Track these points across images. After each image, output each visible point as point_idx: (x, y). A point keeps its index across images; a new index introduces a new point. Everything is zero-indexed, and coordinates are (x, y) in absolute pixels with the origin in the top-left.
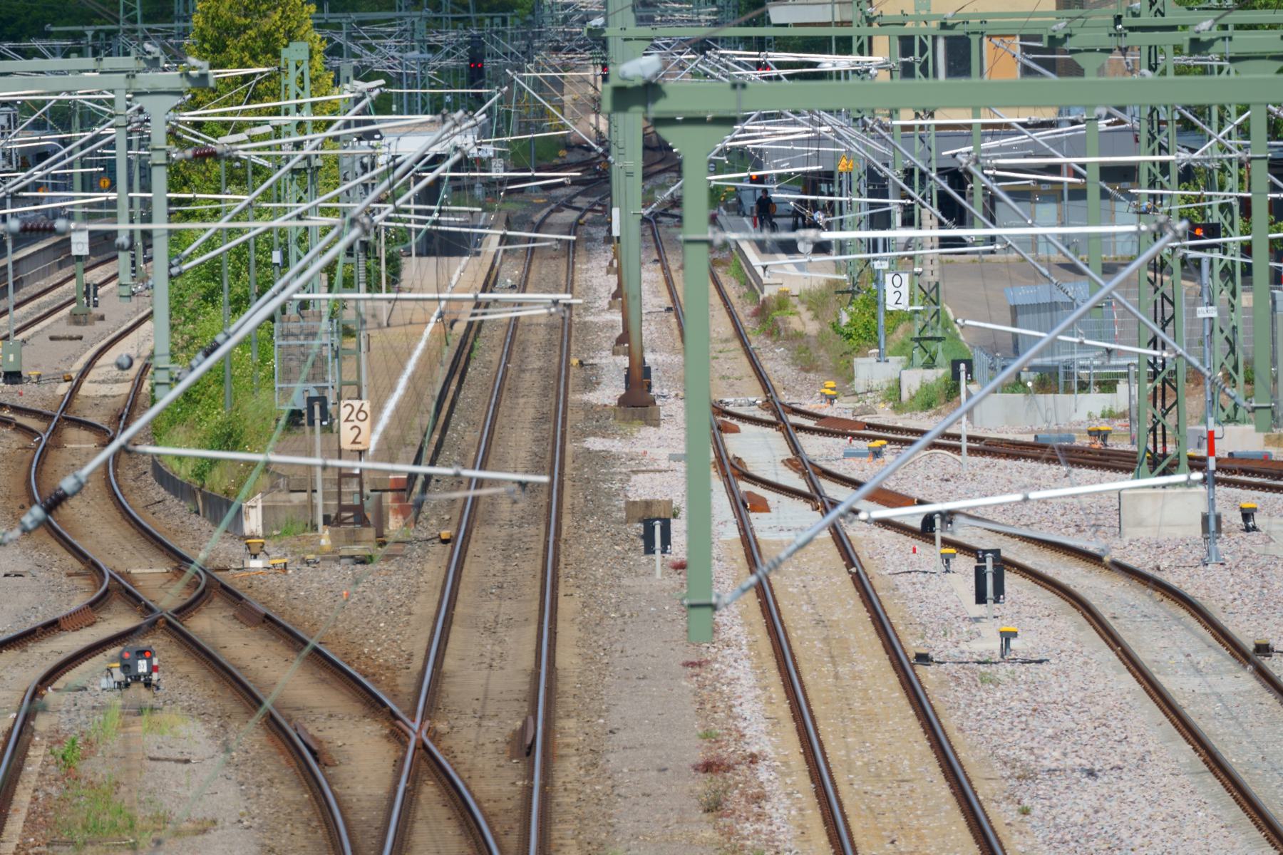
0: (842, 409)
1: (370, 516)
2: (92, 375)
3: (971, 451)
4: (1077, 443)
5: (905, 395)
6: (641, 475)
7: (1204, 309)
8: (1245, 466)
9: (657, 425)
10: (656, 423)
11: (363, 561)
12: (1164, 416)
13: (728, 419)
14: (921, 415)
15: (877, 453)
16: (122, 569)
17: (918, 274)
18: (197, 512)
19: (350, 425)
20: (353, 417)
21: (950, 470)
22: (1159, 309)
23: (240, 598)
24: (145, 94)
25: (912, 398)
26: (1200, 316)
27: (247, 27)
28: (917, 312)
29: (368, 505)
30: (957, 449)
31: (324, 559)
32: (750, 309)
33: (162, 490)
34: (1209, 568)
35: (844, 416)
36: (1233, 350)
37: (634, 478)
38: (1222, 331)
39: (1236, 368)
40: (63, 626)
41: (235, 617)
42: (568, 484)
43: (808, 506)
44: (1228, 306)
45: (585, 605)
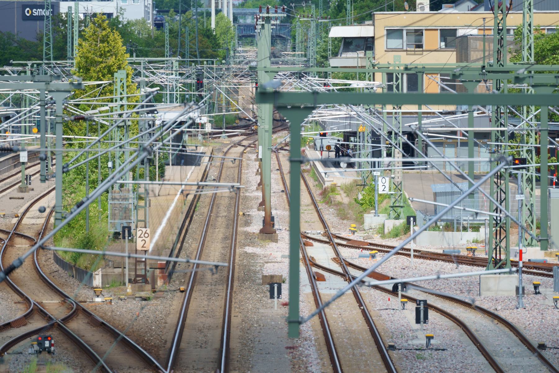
0: (358, 237)
2: (28, 215)
3: (415, 256)
4: (462, 254)
5: (386, 231)
6: (269, 264)
7: (519, 196)
8: (535, 265)
9: (277, 242)
10: (276, 241)
11: (145, 299)
12: (500, 242)
13: (308, 240)
15: (373, 256)
16: (39, 301)
17: (393, 178)
18: (73, 276)
19: (141, 239)
20: (142, 236)
21: (405, 264)
22: (499, 195)
25: (390, 233)
27: (102, 62)
28: (392, 194)
29: (148, 274)
30: (409, 255)
31: (128, 298)
33: (57, 266)
34: (519, 310)
36: (531, 214)
38: (526, 206)
39: (532, 222)
40: (12, 325)
41: (88, 323)
44: (529, 195)
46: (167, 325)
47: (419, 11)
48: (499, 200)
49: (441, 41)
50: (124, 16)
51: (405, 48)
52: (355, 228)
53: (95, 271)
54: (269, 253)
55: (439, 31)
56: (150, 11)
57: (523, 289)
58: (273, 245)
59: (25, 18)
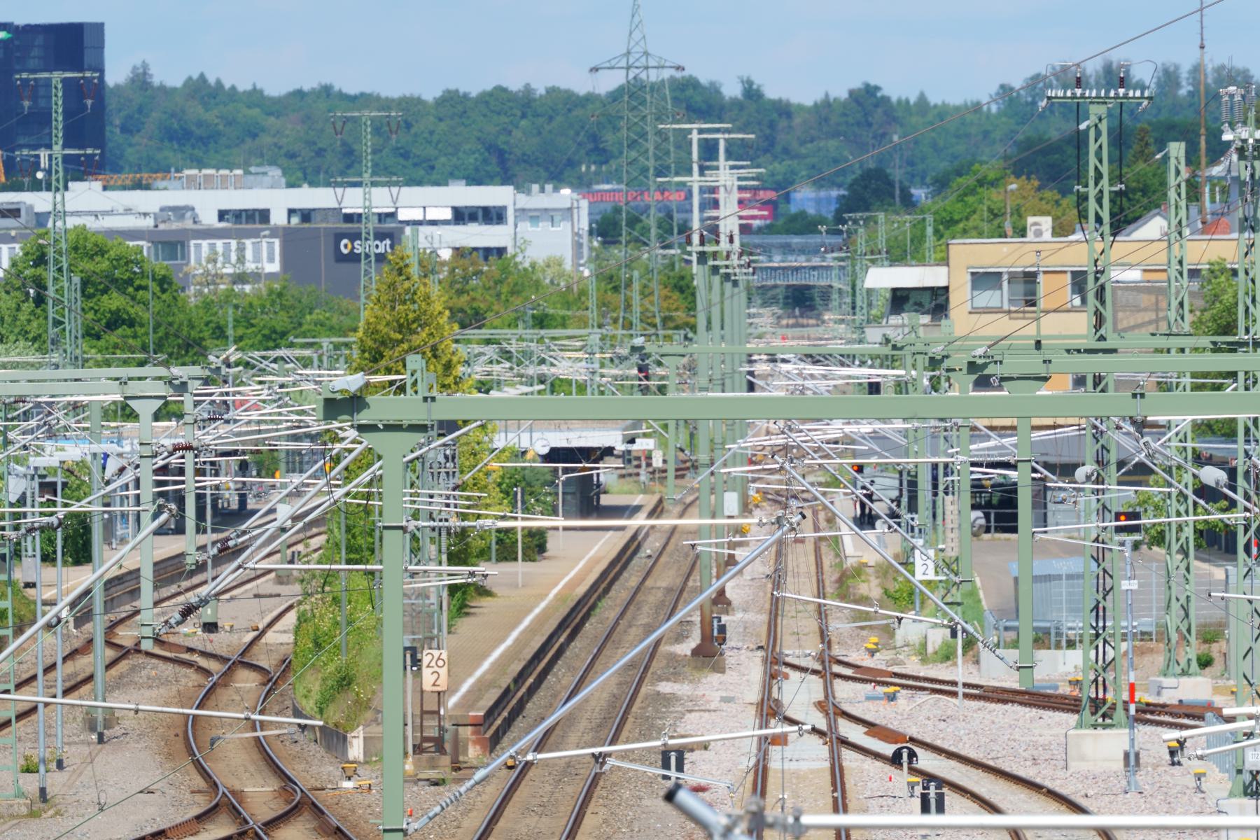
0: (878, 662)
1: (448, 747)
3: (966, 696)
4: (1060, 691)
5: (930, 650)
6: (693, 714)
10: (721, 669)
12: (1104, 670)
14: (940, 666)
15: (892, 698)
16: (238, 787)
17: (942, 550)
19: (431, 670)
20: (433, 664)
22: (1101, 581)
23: (323, 813)
24: (1011, 379)
25: (936, 653)
26: (1124, 588)
27: (402, 341)
29: (447, 736)
30: (954, 694)
32: (836, 576)
34: (1128, 796)
35: (879, 667)
36: (1187, 615)
37: (688, 715)
38: (1178, 600)
39: (1189, 631)
40: (169, 835)
41: (315, 829)
42: (631, 719)
43: (821, 741)
45: (605, 821)
46: (460, 831)
47: (1030, 236)
48: (1101, 589)
49: (1073, 292)
50: (527, 254)
51: (1006, 307)
52: (876, 644)
53: (352, 730)
54: (701, 693)
55: (1069, 276)
56: (585, 240)
57: (1137, 755)
58: (715, 678)
59: (341, 258)
